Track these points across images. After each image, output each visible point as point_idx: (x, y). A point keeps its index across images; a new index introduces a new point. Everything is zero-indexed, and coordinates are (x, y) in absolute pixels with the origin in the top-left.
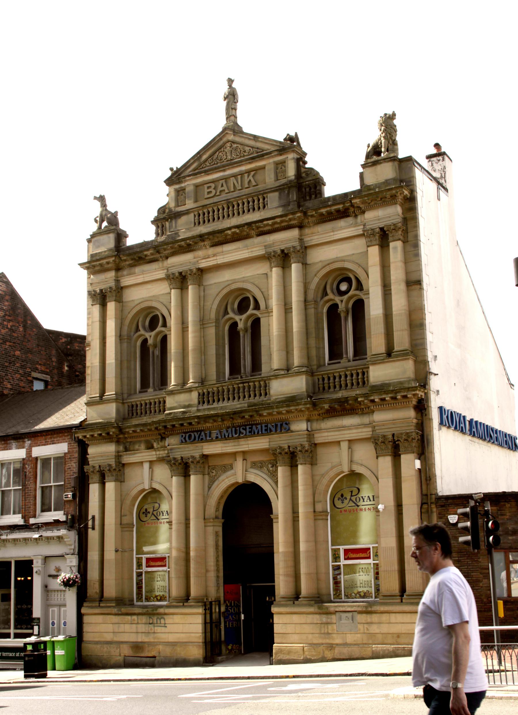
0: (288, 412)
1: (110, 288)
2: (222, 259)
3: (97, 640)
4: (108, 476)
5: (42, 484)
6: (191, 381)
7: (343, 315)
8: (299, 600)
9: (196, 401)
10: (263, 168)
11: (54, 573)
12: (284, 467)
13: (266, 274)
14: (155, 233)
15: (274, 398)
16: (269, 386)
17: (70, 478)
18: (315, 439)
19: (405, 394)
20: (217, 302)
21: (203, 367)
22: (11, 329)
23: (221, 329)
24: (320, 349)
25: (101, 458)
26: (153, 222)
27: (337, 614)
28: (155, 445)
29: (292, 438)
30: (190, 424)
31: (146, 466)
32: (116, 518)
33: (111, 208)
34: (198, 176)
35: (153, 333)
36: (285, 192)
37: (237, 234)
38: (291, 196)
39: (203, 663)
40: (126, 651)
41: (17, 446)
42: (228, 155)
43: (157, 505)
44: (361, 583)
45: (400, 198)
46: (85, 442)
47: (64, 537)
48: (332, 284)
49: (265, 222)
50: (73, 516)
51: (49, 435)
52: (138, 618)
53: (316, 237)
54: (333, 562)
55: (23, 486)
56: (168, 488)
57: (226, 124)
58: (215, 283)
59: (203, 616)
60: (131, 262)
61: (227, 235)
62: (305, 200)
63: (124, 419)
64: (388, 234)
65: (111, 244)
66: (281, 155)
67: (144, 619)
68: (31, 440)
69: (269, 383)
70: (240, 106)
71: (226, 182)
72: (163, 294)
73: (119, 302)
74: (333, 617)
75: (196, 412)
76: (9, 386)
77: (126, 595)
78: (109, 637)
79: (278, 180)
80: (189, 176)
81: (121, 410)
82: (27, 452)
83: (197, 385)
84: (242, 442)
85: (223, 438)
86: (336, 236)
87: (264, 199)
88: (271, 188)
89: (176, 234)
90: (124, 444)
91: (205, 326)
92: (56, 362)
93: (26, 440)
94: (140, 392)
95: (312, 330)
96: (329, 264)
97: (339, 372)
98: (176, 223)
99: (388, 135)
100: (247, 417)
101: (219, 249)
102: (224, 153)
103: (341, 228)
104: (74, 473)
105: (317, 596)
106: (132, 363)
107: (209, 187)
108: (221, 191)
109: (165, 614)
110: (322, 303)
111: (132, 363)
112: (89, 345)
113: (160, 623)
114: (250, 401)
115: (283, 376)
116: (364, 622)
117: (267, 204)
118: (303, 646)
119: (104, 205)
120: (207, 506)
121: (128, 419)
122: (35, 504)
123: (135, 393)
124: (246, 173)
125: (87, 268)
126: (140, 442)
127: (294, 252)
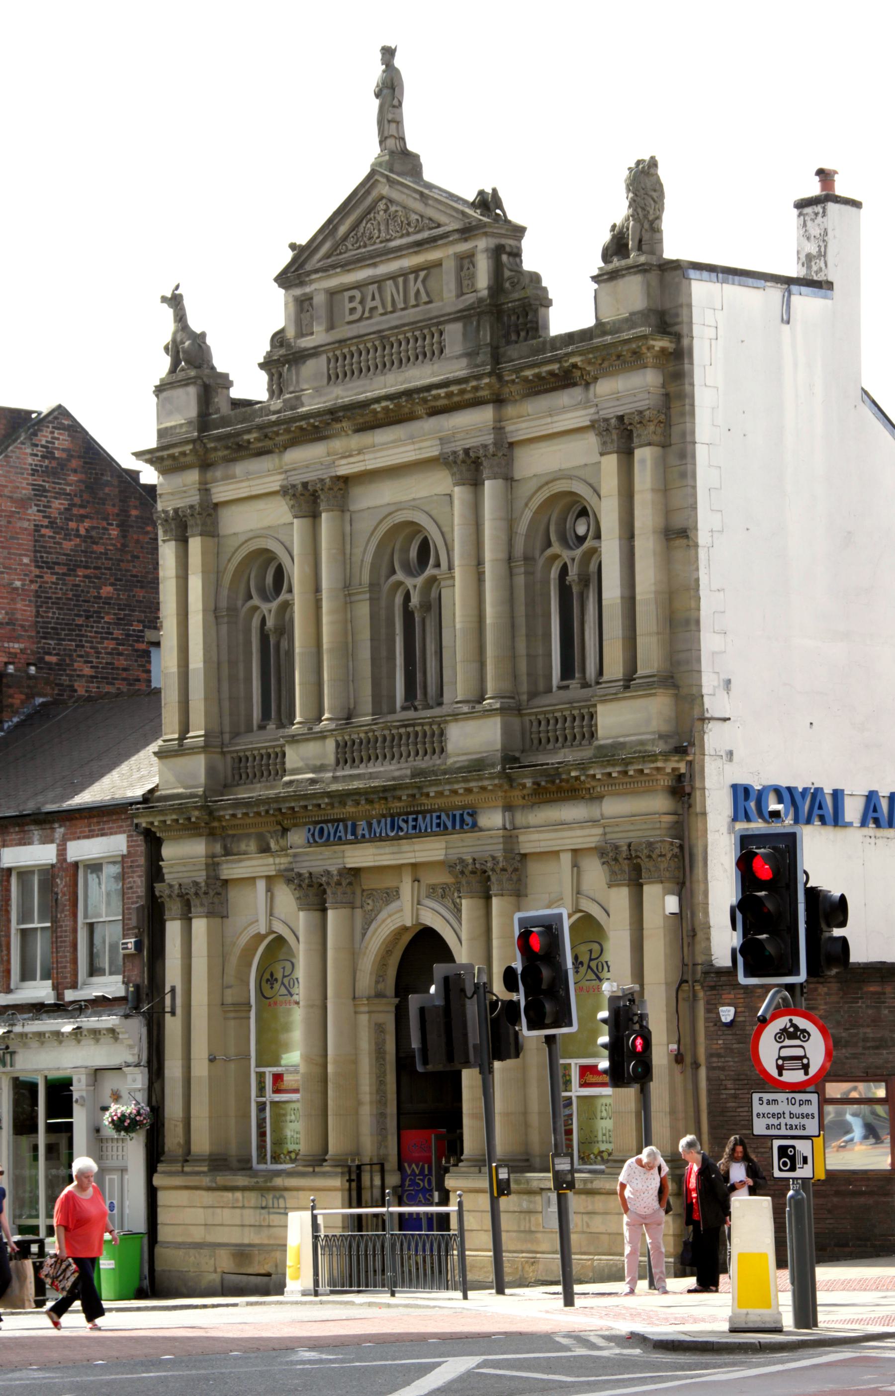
0: (469, 791)
1: (192, 507)
2: (373, 461)
3: (180, 1240)
9: (331, 759)
10: (438, 264)
12: (469, 900)
14: (268, 390)
19: (640, 767)
21: (351, 683)
22: (86, 537)
23: (383, 603)
25: (184, 869)
26: (262, 366)
27: (544, 1193)
28: (273, 845)
29: (480, 842)
31: (261, 885)
33: (196, 324)
34: (331, 272)
36: (472, 323)
38: (481, 333)
40: (225, 1262)
41: (41, 836)
44: (604, 1135)
45: (649, 358)
47: (118, 1030)
49: (434, 392)
50: (137, 987)
51: (94, 817)
52: (243, 1197)
53: (524, 425)
55: (52, 923)
57: (379, 156)
58: (369, 508)
59: (346, 1194)
61: (375, 412)
62: (508, 343)
63: (226, 787)
65: (192, 412)
66: (466, 240)
67: (252, 1198)
72: (285, 524)
73: (213, 537)
74: (538, 1198)
75: (331, 783)
76: (87, 671)
77: (233, 1150)
78: (198, 1235)
79: (463, 294)
80: (316, 271)
82: (58, 850)
84: (405, 845)
86: (555, 425)
88: (449, 314)
89: (298, 398)
91: (354, 598)
93: (56, 825)
95: (521, 621)
96: (547, 483)
98: (298, 374)
99: (639, 210)
100: (404, 798)
102: (375, 223)
103: (565, 409)
104: (138, 897)
105: (524, 1157)
106: (241, 666)
107: (352, 299)
108: (373, 309)
109: (286, 1189)
110: (541, 562)
111: (241, 666)
113: (279, 1208)
114: (415, 763)
116: (582, 1210)
119: (180, 317)
122: (75, 961)
124: (412, 272)
126: (248, 836)
127: (485, 456)
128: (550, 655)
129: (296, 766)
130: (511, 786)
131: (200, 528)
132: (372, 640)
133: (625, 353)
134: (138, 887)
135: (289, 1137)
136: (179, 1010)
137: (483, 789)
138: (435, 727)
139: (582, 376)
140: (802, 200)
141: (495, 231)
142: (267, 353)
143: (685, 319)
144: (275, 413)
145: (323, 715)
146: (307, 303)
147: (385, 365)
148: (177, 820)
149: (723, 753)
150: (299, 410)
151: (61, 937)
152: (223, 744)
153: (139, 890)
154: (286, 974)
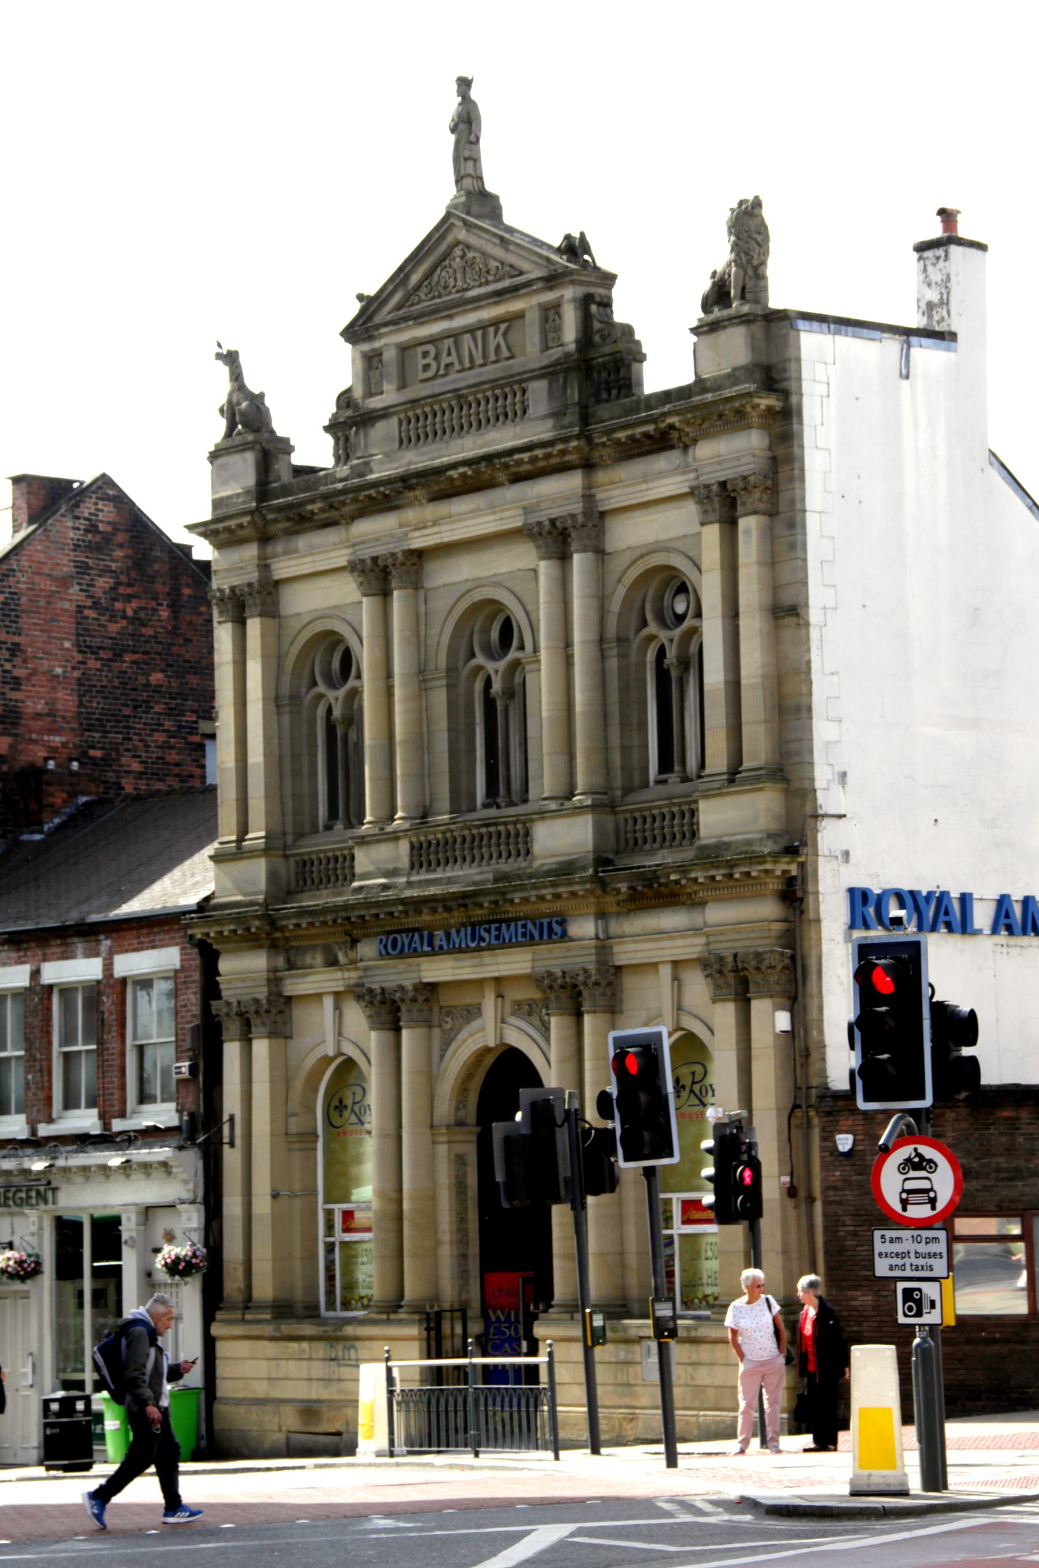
0: (557, 897)
1: (250, 585)
3: (240, 1395)
4: (256, 1025)
8: (551, 1310)
9: (405, 862)
10: (520, 316)
18: (616, 957)
20: (449, 629)
21: (426, 779)
22: (133, 619)
24: (638, 749)
28: (341, 957)
29: (568, 954)
31: (328, 1002)
33: (253, 385)
34: (403, 325)
36: (558, 380)
38: (569, 391)
40: (291, 1420)
41: (85, 949)
43: (359, 1090)
44: (709, 1277)
45: (754, 418)
49: (517, 457)
50: (192, 1115)
52: (311, 1348)
53: (616, 492)
57: (455, 197)
58: (445, 585)
59: (424, 1343)
61: (451, 479)
62: (599, 402)
63: (289, 894)
65: (250, 480)
66: (551, 289)
67: (320, 1349)
68: (111, 938)
71: (456, 344)
73: (274, 617)
74: (637, 1348)
75: (405, 889)
76: (136, 766)
77: (299, 1295)
78: (260, 1390)
79: (547, 348)
80: (386, 324)
81: (283, 871)
84: (487, 957)
86: (654, 491)
88: (533, 371)
89: (366, 464)
90: (287, 951)
91: (429, 685)
93: (102, 937)
96: (642, 556)
97: (660, 807)
99: (742, 255)
100: (486, 905)
102: (451, 271)
103: (661, 475)
104: (193, 1016)
105: (621, 1302)
106: (305, 760)
107: (425, 354)
108: (448, 366)
109: (357, 1339)
110: (636, 643)
111: (305, 760)
113: (349, 1359)
114: (498, 867)
115: (557, 814)
119: (237, 376)
120: (436, 1098)
122: (123, 1087)
124: (491, 325)
126: (314, 948)
131: (259, 608)
132: (450, 730)
133: (727, 412)
134: (192, 1005)
136: (238, 1141)
137: (574, 894)
138: (519, 826)
142: (333, 415)
143: (793, 374)
146: (376, 359)
150: (368, 478)
153: (194, 1008)
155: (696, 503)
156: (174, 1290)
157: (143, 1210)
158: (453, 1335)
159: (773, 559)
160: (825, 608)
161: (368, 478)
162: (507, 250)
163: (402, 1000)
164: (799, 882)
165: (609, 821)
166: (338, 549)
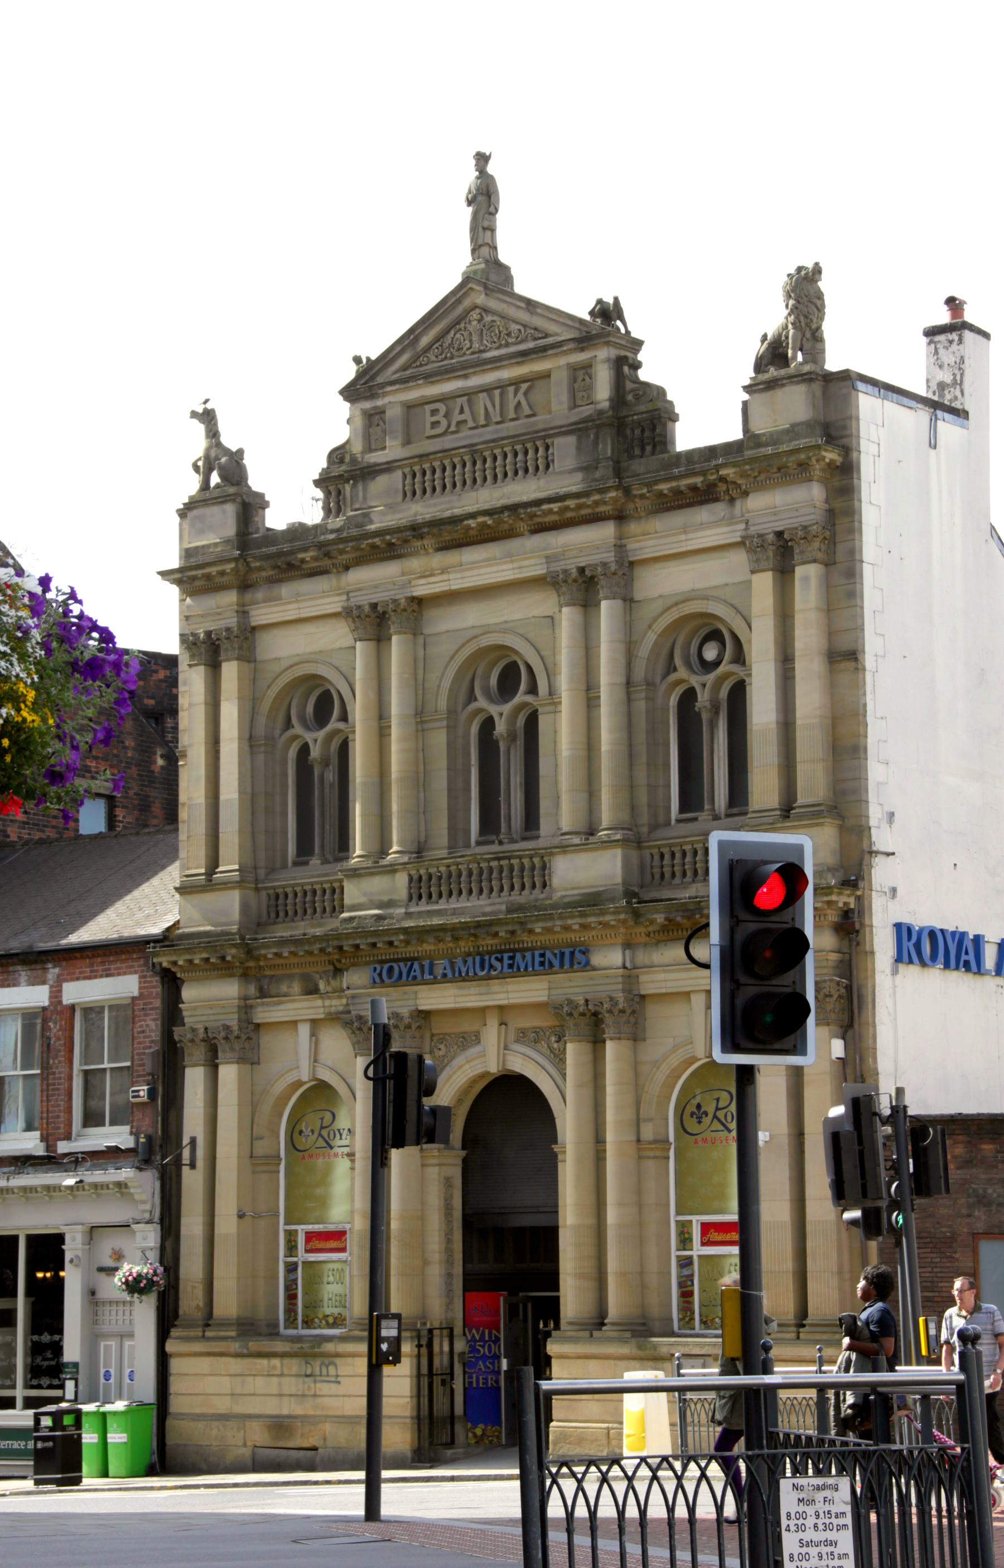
0: (584, 927)
1: (228, 629)
2: (460, 581)
5: (86, 1064)
6: (395, 848)
7: (705, 716)
9: (403, 894)
10: (546, 375)
11: (110, 1263)
12: (577, 1044)
13: (552, 618)
15: (559, 894)
16: (550, 869)
17: (144, 1054)
18: (641, 986)
20: (451, 673)
21: (422, 816)
24: (657, 789)
28: (322, 985)
29: (591, 982)
30: (391, 944)
31: (304, 1030)
32: (240, 1144)
33: (230, 441)
34: (411, 384)
35: (321, 734)
36: (589, 436)
37: (489, 526)
38: (600, 446)
39: (413, 1461)
40: (258, 1435)
41: (29, 977)
42: (474, 339)
43: (328, 1116)
45: (817, 469)
46: (174, 973)
47: (129, 1184)
48: (687, 645)
49: (545, 507)
50: (149, 1138)
51: (99, 956)
52: (282, 1365)
53: (651, 543)
54: (678, 1250)
55: (42, 1069)
56: (349, 1081)
57: (471, 265)
58: (448, 631)
59: (415, 1360)
60: (271, 573)
61: (469, 528)
62: (632, 457)
64: (792, 547)
65: (230, 530)
66: (582, 350)
67: (294, 1365)
68: (59, 966)
69: (550, 861)
70: (503, 221)
71: (470, 402)
72: (341, 648)
73: (249, 662)
75: (403, 919)
77: (262, 1314)
78: (222, 1405)
79: (575, 406)
80: (392, 383)
82: (51, 992)
83: (406, 859)
84: (496, 985)
85: (457, 976)
87: (547, 448)
88: (561, 427)
89: (366, 515)
90: (258, 980)
91: (426, 726)
92: (134, 749)
93: (50, 965)
94: (295, 864)
95: (641, 749)
96: (676, 604)
97: (692, 843)
98: (365, 490)
99: (802, 318)
100: (502, 934)
101: (452, 557)
102: (466, 334)
103: (702, 526)
104: (152, 1042)
106: (278, 799)
107: (434, 412)
108: (459, 423)
109: (338, 1355)
110: (663, 687)
111: (278, 799)
112: (184, 755)
113: (328, 1375)
114: (512, 898)
115: (578, 848)
117: (553, 461)
118: (608, 1428)
119: (213, 433)
121: (267, 924)
122: (69, 1110)
123: (284, 866)
125: (178, 582)
126: (291, 977)
127: (605, 574)
128: (669, 786)
129: (356, 901)
130: (636, 923)
131: (236, 652)
132: (449, 769)
133: (790, 464)
135: (326, 1298)
136: (200, 1163)
137: (606, 925)
138: (536, 861)
139: (728, 490)
140: (933, 327)
141: (618, 341)
142: (323, 469)
143: (854, 432)
144: (332, 531)
145: (391, 848)
146: (377, 417)
147: (475, 481)
148: (207, 960)
149: (887, 890)
150: (368, 527)
151: (54, 1084)
152: (257, 880)
153: (153, 1034)
154: (720, 1106)
155: (747, 552)
156: (127, 1308)
157: (88, 1229)
158: (441, 1352)
159: (828, 606)
160: (876, 656)
161: (368, 527)
162: (532, 313)
163: (396, 1027)
164: (856, 915)
165: (634, 854)
166: (328, 596)
